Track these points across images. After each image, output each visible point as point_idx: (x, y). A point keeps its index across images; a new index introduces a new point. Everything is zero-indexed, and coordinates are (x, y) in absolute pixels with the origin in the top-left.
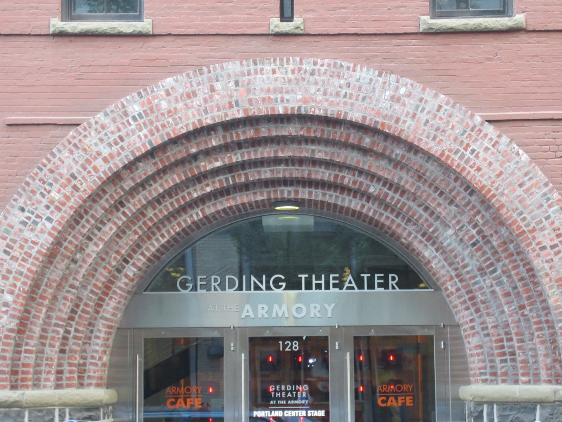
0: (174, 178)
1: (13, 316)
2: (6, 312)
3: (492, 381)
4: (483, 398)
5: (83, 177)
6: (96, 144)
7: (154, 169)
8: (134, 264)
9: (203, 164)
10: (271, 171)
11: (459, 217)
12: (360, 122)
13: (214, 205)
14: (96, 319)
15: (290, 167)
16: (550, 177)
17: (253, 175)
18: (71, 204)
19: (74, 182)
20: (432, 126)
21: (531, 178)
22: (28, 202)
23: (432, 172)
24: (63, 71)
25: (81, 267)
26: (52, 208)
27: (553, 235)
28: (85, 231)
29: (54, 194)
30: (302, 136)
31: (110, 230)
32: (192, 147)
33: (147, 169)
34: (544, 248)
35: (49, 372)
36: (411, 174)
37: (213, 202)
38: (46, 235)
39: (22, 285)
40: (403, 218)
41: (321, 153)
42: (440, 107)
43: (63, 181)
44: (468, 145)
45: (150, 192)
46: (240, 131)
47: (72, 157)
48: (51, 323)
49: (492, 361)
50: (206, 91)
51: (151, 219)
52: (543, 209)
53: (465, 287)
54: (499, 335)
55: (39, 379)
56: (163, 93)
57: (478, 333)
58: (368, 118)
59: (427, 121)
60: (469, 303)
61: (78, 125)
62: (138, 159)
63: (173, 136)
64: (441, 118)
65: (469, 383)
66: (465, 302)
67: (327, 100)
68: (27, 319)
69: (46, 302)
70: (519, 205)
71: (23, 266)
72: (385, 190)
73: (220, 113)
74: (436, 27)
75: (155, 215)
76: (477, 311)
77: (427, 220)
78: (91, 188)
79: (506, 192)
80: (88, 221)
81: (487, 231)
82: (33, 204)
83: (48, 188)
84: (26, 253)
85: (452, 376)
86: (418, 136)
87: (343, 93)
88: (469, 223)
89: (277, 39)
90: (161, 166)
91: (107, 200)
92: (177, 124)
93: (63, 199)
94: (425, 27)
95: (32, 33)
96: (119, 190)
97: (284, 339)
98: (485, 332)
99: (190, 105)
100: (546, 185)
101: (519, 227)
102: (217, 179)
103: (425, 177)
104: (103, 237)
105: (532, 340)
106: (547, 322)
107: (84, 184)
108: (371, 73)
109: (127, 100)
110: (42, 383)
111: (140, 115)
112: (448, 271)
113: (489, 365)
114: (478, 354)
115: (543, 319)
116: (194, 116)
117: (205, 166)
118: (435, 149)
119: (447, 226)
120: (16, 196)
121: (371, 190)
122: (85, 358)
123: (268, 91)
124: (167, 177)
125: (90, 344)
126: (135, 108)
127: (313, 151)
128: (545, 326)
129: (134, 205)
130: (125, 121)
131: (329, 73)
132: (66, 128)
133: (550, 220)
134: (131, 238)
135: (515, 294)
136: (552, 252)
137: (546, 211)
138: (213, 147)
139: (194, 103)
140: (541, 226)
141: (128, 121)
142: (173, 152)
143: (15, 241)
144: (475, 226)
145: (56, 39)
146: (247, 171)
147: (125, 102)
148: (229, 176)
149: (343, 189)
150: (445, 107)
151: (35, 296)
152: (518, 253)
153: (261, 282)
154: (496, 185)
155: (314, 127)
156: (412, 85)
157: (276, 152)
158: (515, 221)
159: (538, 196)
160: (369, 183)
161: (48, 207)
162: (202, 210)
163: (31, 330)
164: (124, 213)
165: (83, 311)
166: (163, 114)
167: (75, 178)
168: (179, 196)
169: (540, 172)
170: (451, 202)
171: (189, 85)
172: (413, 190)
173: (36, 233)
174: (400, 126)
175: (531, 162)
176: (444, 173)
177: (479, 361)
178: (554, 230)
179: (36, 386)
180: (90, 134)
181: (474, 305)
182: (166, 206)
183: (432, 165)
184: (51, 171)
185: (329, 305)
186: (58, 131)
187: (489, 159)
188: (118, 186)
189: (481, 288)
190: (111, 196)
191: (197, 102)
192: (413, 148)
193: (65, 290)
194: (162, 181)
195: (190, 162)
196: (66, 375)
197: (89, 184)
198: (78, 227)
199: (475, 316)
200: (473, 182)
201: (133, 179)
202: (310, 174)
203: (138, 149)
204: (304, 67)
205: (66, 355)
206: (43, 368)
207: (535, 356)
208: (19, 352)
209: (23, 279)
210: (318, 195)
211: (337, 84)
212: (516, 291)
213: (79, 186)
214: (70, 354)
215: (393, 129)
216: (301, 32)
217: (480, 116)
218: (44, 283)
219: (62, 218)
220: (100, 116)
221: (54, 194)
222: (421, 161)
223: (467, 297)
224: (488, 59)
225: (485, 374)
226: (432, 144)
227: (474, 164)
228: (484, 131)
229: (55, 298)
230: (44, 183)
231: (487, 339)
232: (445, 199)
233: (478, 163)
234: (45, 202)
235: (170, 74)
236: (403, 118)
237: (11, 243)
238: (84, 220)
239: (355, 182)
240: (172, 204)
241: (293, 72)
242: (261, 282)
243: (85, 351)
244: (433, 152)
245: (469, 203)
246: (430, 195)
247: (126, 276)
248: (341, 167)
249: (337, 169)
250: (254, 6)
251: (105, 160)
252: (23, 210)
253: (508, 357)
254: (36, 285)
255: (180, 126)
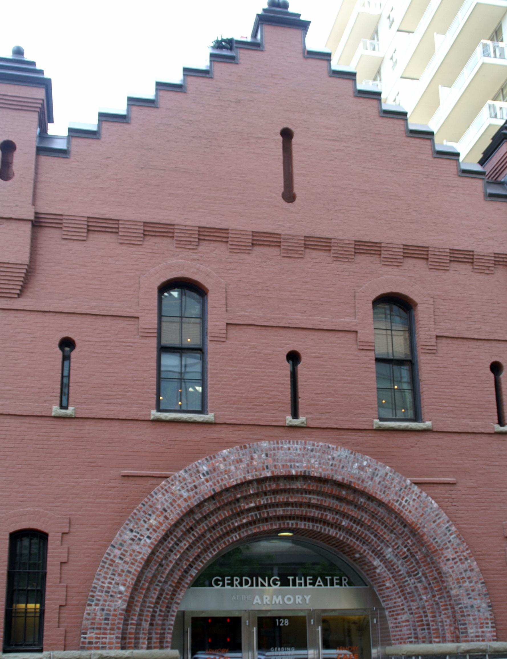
0: (225, 514)
1: (125, 601)
2: (120, 598)
3: (415, 642)
4: (413, 652)
5: (171, 511)
6: (179, 490)
7: (215, 507)
8: (196, 568)
9: (243, 504)
10: (283, 510)
11: (396, 541)
12: (341, 481)
13: (247, 531)
14: (171, 603)
15: (295, 508)
16: (449, 517)
17: (272, 512)
18: (163, 528)
19: (165, 514)
20: (383, 485)
21: (439, 518)
22: (136, 526)
23: (382, 513)
24: (158, 443)
25: (165, 569)
26: (151, 530)
27: (453, 552)
28: (170, 545)
29: (152, 521)
30: (305, 489)
31: (184, 545)
32: (238, 494)
33: (210, 507)
34: (448, 560)
35: (144, 638)
36: (368, 514)
37: (245, 529)
38: (147, 548)
39: (130, 581)
40: (361, 541)
41: (314, 499)
42: (387, 474)
43: (158, 513)
44: (403, 497)
45: (210, 522)
46: (267, 484)
47: (164, 498)
48: (146, 606)
49: (415, 630)
50: (248, 459)
51: (208, 539)
52: (447, 536)
53: (397, 584)
54: (420, 613)
55: (138, 643)
56: (221, 459)
57: (406, 612)
58: (346, 479)
59: (380, 482)
60: (400, 594)
61: (168, 477)
62: (205, 500)
63: (228, 486)
64: (388, 481)
65: (390, 644)
66: (398, 593)
67: (321, 467)
68: (133, 602)
69: (144, 592)
70: (433, 534)
71: (132, 568)
72: (352, 524)
73: (257, 473)
74: (383, 427)
75: (211, 536)
76: (405, 598)
77: (376, 542)
78: (176, 518)
79: (426, 526)
80: (172, 539)
81: (414, 549)
82: (138, 527)
83: (148, 517)
84: (133, 559)
85: (382, 641)
86: (375, 491)
87: (331, 463)
88: (402, 544)
89: (290, 429)
90: (218, 505)
91: (184, 526)
92: (230, 479)
93: (158, 525)
94: (377, 426)
95: (139, 419)
96: (192, 520)
97: (279, 618)
98: (411, 612)
99: (238, 467)
100: (448, 522)
101: (434, 547)
102: (250, 514)
103: (376, 516)
104: (180, 550)
105: (440, 616)
106: (450, 605)
107: (172, 515)
108: (347, 452)
109: (199, 463)
110: (140, 645)
111: (207, 473)
112: (388, 574)
113: (413, 632)
114: (407, 626)
115: (448, 603)
116: (241, 474)
117: (244, 506)
118: (385, 500)
119: (388, 546)
120: (127, 522)
121: (343, 523)
122: (165, 629)
123: (286, 460)
124: (220, 512)
125: (167, 620)
126: (205, 468)
127: (310, 499)
128: (449, 607)
129: (200, 530)
130: (197, 476)
131: (321, 451)
132: (160, 479)
133: (451, 543)
134: (196, 551)
135: (429, 588)
136: (453, 562)
137: (449, 538)
138: (251, 494)
139: (241, 466)
140: (446, 546)
141: (199, 476)
142: (226, 497)
143: (126, 551)
144: (405, 547)
145: (154, 423)
146: (269, 510)
147: (197, 464)
148: (257, 513)
149: (325, 522)
150: (390, 474)
151: (137, 587)
152: (433, 563)
153: (265, 581)
154: (420, 521)
155: (312, 484)
156: (370, 460)
157: (288, 498)
158: (432, 544)
159: (444, 528)
160: (341, 519)
161: (148, 530)
162: (239, 534)
163: (135, 610)
164: (193, 535)
165: (165, 598)
166: (221, 473)
167: (166, 511)
168: (226, 525)
169: (444, 515)
170: (392, 532)
171: (237, 455)
172: (369, 524)
173: (140, 546)
174: (365, 484)
175: (439, 509)
176: (389, 514)
177: (407, 630)
178: (454, 549)
179: (136, 647)
180: (175, 483)
181: (403, 595)
182: (218, 531)
183: (382, 509)
184: (151, 507)
185: (307, 596)
186: (154, 481)
187: (416, 506)
188: (192, 517)
189: (409, 584)
190: (187, 523)
191: (243, 466)
192: (371, 498)
193: (155, 584)
194: (218, 515)
195: (235, 503)
196: (154, 640)
197: (173, 516)
198: (166, 543)
199: (404, 602)
200: (407, 519)
201: (201, 513)
202: (306, 512)
203: (206, 494)
204: (307, 446)
205: (154, 627)
206: (141, 636)
207: (442, 626)
208: (127, 625)
209: (131, 576)
210: (309, 525)
211: (326, 458)
212: (430, 586)
213: (168, 516)
214: (156, 627)
215: (359, 486)
216: (305, 426)
217: (410, 480)
218: (143, 579)
219: (158, 536)
220: (182, 472)
221: (152, 521)
222: (375, 506)
223: (399, 590)
224: (412, 447)
225: (411, 638)
226: (383, 496)
227: (408, 508)
228: (412, 489)
229: (148, 589)
230: (146, 514)
231: (411, 616)
232: (388, 530)
233: (410, 508)
234: (146, 526)
235: (226, 448)
236: (366, 480)
237: (124, 553)
238: (169, 538)
239: (333, 519)
240: (222, 530)
241: (300, 449)
242: (265, 581)
243: (164, 624)
244: (384, 501)
245: (403, 532)
246: (379, 527)
247: (191, 575)
248: (325, 509)
249: (323, 510)
250: (276, 408)
251: (185, 500)
252: (132, 531)
253: (425, 627)
254: (138, 581)
255: (232, 480)
